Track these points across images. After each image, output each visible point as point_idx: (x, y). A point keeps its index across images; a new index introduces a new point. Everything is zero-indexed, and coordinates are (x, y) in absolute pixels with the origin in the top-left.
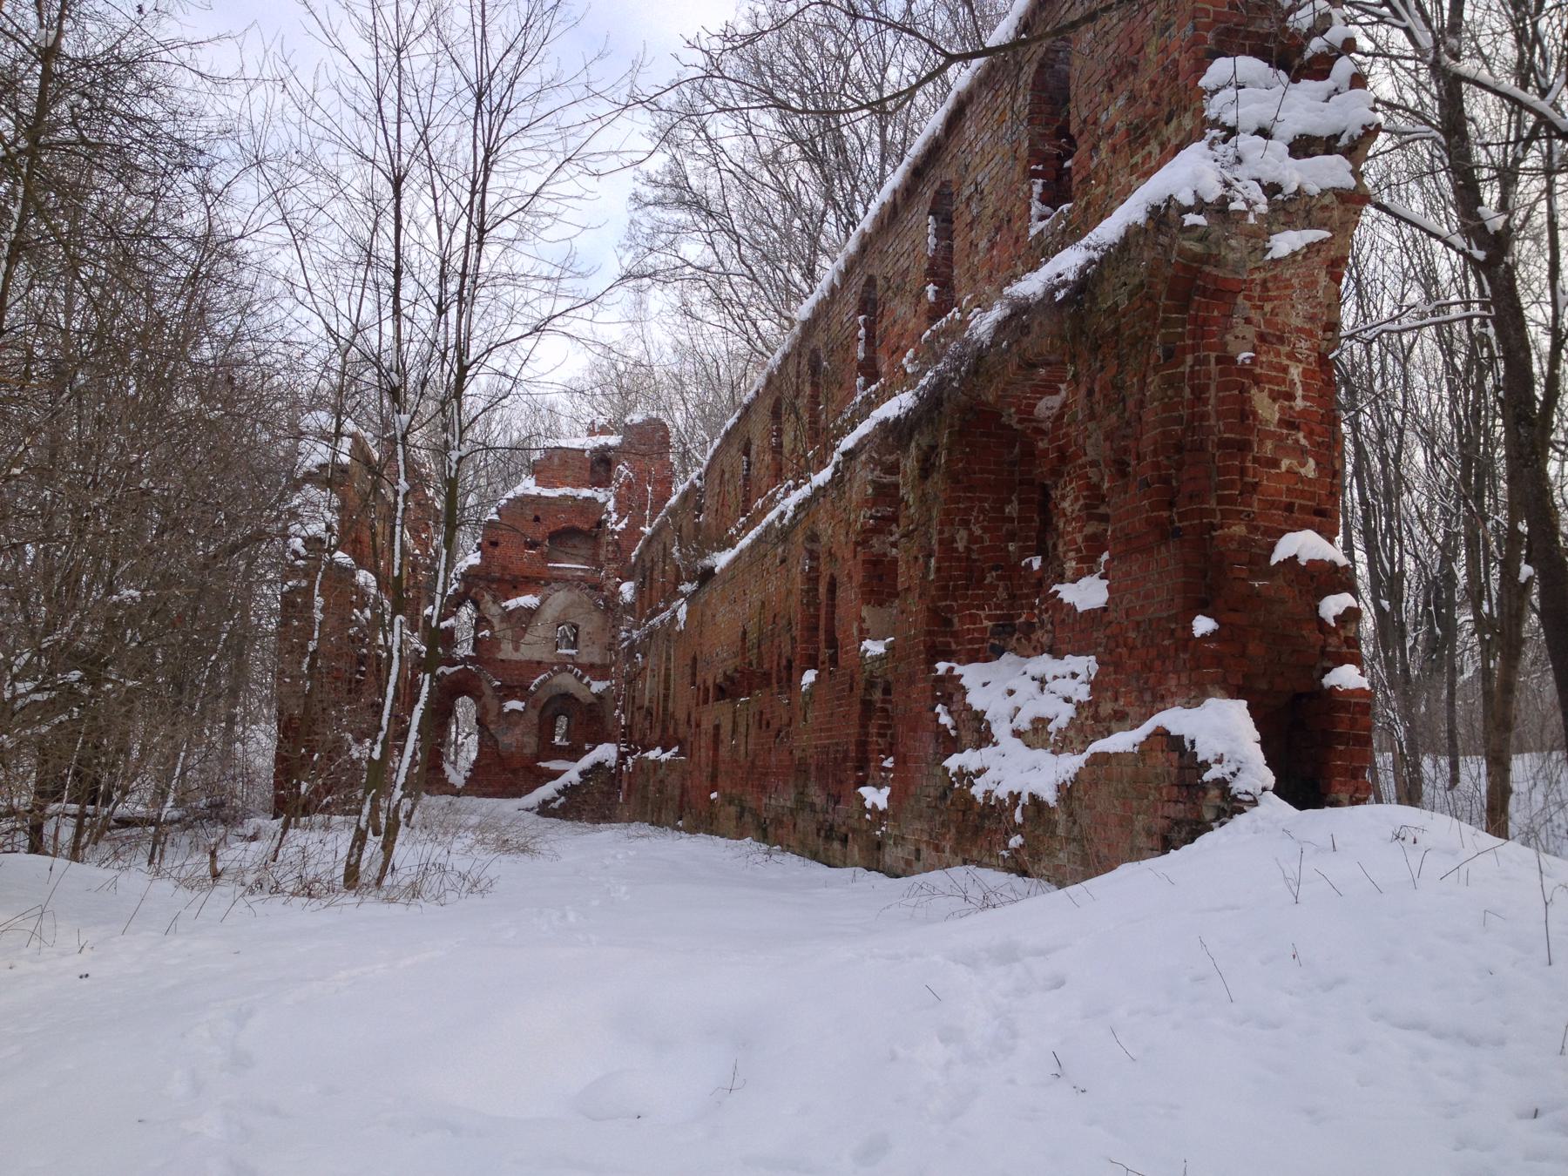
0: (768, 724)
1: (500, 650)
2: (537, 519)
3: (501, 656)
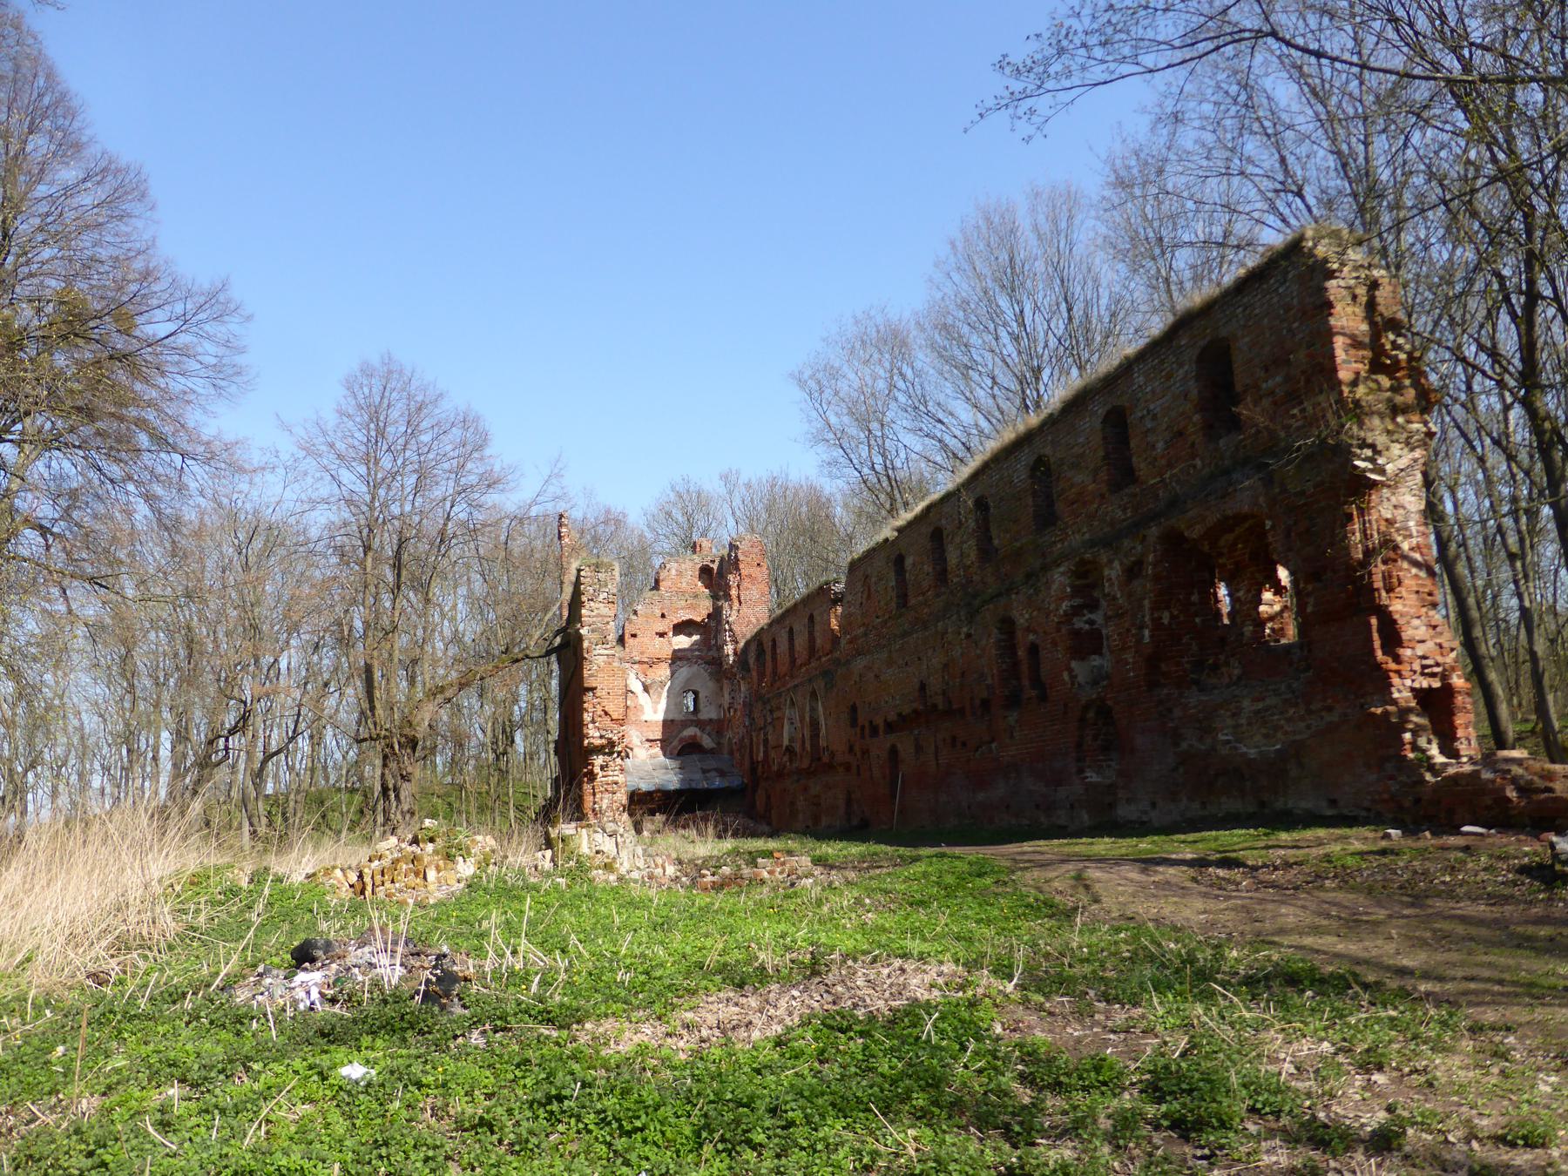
0: (964, 744)
1: (642, 711)
2: (663, 616)
3: (644, 718)
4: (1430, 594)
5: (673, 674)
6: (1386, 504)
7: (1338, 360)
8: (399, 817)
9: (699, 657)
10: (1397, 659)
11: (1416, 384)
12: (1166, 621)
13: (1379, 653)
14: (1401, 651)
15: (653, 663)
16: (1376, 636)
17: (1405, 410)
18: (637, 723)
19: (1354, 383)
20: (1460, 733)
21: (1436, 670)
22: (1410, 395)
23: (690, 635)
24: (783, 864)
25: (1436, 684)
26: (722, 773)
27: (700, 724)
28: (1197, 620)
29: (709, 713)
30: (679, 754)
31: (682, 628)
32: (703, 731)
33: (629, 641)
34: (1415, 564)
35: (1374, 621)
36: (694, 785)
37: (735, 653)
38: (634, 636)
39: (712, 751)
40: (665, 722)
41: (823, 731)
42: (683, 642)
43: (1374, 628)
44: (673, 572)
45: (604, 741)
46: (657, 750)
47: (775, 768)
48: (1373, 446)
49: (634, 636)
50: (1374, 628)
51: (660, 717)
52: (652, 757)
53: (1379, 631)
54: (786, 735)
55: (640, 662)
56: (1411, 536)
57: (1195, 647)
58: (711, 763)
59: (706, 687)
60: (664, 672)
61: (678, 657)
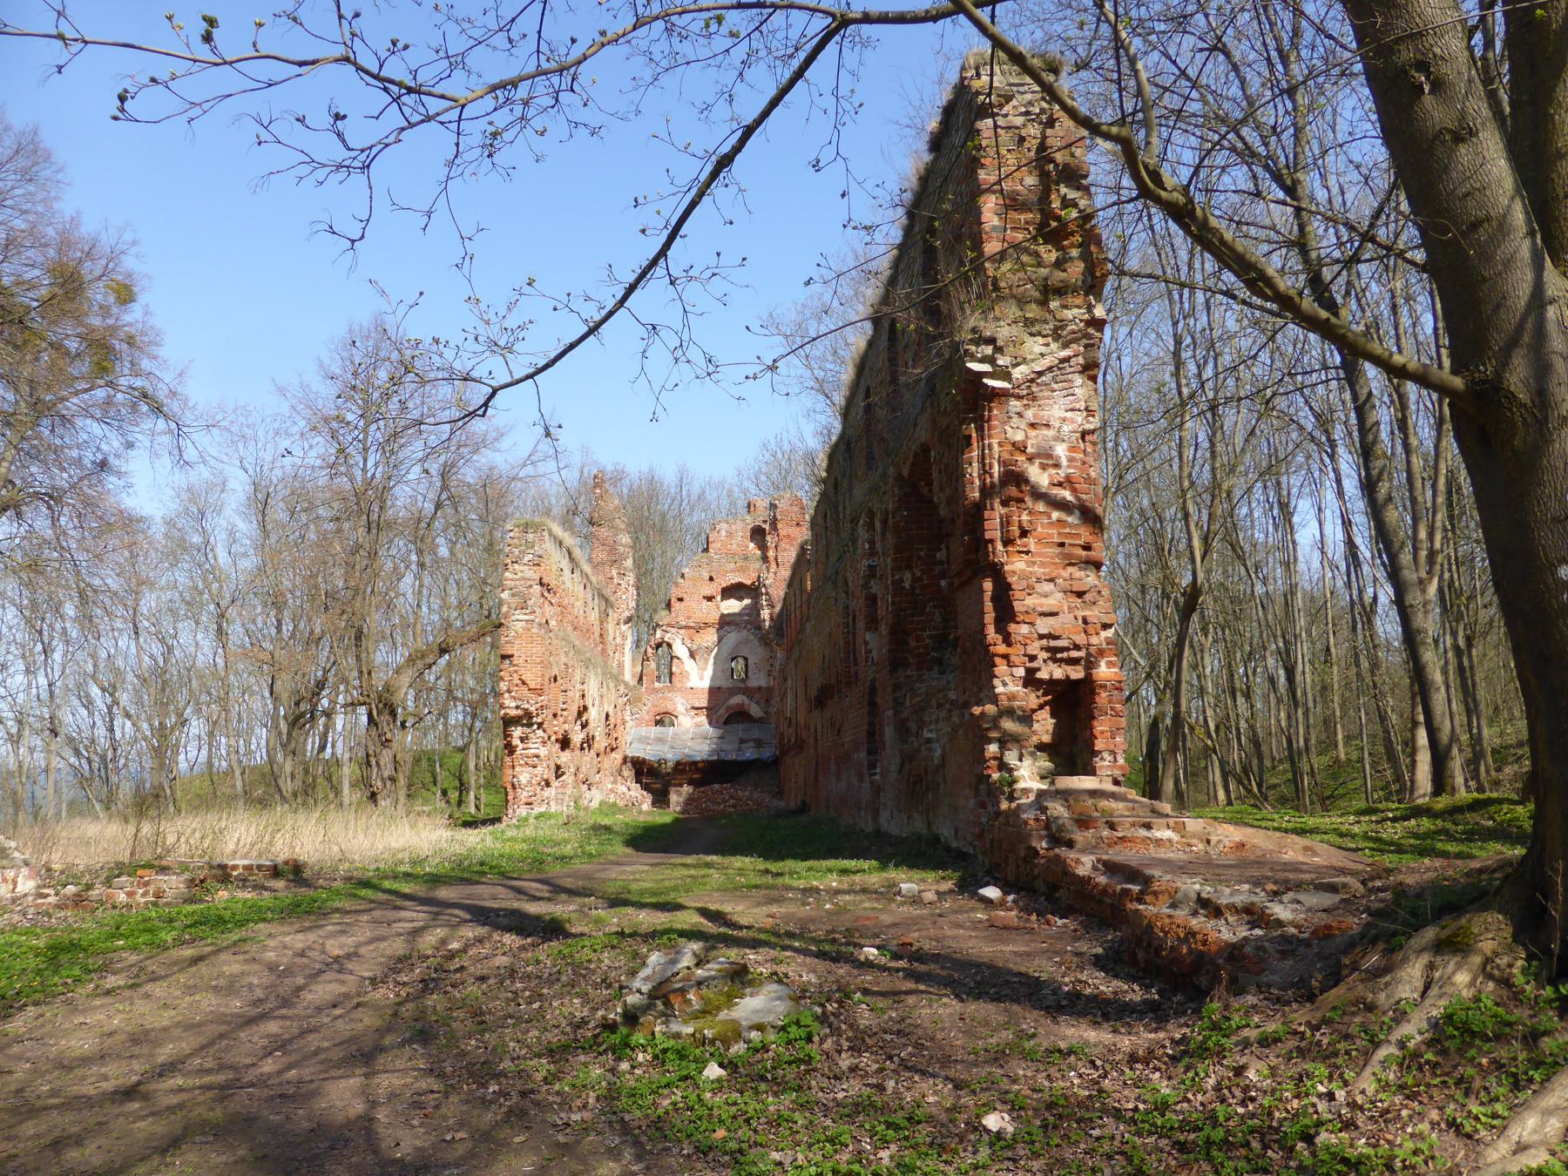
2: (711, 579)
3: (690, 685)
4: (1087, 548)
5: (720, 640)
6: (1015, 420)
7: (986, 227)
8: (379, 784)
9: (747, 622)
10: (1008, 641)
11: (1086, 257)
12: (907, 585)
13: (991, 630)
14: (1012, 627)
15: (699, 628)
16: (988, 606)
17: (1060, 291)
18: (683, 690)
19: (1001, 256)
20: (1099, 745)
21: (1074, 654)
22: (1076, 270)
23: (740, 599)
24: (146, 884)
25: (1077, 673)
26: (759, 744)
27: (749, 692)
28: (943, 583)
29: (758, 680)
30: (726, 723)
31: (731, 591)
32: (751, 698)
33: (676, 606)
34: (1062, 505)
35: (988, 585)
38: (681, 600)
39: (760, 721)
42: (733, 606)
43: (988, 595)
44: (723, 533)
45: (520, 712)
46: (703, 719)
48: (991, 341)
49: (681, 600)
50: (988, 595)
51: (706, 684)
52: (698, 725)
53: (993, 599)
55: (686, 627)
56: (1057, 466)
57: (938, 618)
58: (756, 733)
59: (756, 654)
60: (710, 637)
61: (725, 622)
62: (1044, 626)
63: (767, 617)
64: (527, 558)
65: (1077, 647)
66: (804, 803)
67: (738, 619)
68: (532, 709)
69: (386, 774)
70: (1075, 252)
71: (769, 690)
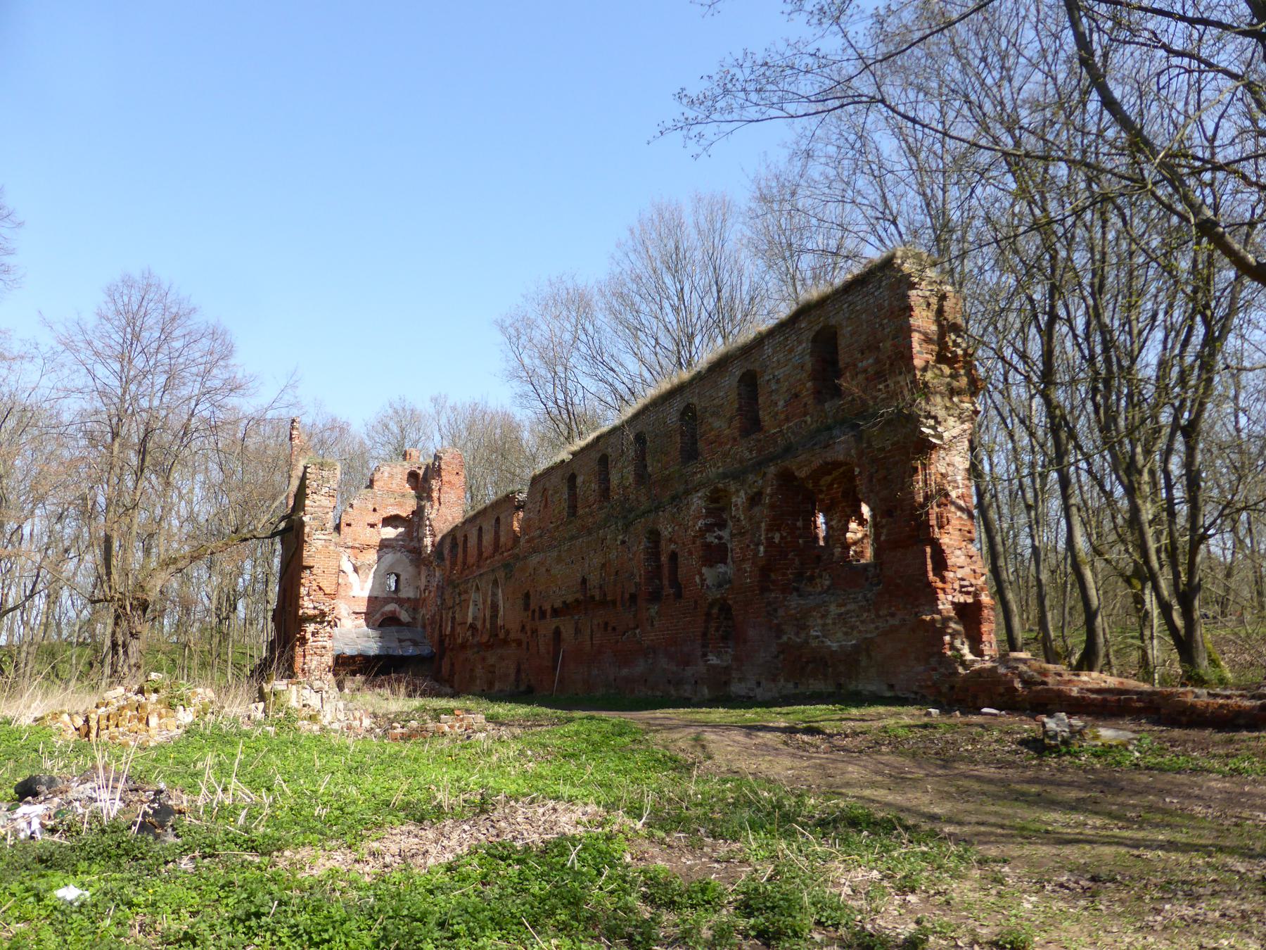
2: (375, 510)
3: (352, 594)
5: (379, 558)
6: (942, 462)
8: (126, 669)
9: (402, 546)
10: (943, 580)
12: (777, 541)
16: (929, 561)
17: (959, 392)
20: (985, 638)
22: (964, 381)
23: (396, 527)
25: (970, 600)
26: (415, 643)
27: (400, 602)
28: (801, 541)
31: (390, 521)
32: (401, 606)
33: (344, 529)
35: (928, 550)
36: (391, 652)
37: (433, 545)
38: (349, 525)
39: (408, 625)
40: (370, 599)
41: (501, 612)
42: (390, 533)
43: (928, 555)
44: (386, 474)
45: (317, 612)
46: (362, 622)
47: (460, 641)
48: (935, 418)
49: (349, 525)
50: (928, 555)
52: (356, 627)
53: (932, 557)
54: (470, 614)
59: (407, 572)
60: (372, 556)
61: (384, 545)
62: (960, 573)
63: (429, 544)
64: (325, 490)
65: (972, 585)
66: (528, 686)
67: (394, 543)
68: (326, 610)
69: (132, 662)
70: (962, 372)
71: (416, 601)
